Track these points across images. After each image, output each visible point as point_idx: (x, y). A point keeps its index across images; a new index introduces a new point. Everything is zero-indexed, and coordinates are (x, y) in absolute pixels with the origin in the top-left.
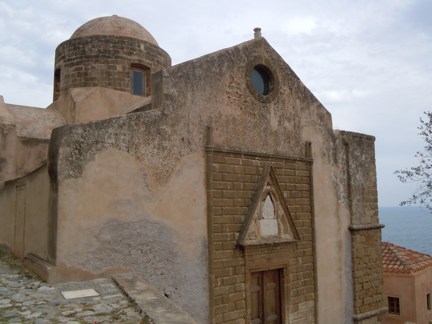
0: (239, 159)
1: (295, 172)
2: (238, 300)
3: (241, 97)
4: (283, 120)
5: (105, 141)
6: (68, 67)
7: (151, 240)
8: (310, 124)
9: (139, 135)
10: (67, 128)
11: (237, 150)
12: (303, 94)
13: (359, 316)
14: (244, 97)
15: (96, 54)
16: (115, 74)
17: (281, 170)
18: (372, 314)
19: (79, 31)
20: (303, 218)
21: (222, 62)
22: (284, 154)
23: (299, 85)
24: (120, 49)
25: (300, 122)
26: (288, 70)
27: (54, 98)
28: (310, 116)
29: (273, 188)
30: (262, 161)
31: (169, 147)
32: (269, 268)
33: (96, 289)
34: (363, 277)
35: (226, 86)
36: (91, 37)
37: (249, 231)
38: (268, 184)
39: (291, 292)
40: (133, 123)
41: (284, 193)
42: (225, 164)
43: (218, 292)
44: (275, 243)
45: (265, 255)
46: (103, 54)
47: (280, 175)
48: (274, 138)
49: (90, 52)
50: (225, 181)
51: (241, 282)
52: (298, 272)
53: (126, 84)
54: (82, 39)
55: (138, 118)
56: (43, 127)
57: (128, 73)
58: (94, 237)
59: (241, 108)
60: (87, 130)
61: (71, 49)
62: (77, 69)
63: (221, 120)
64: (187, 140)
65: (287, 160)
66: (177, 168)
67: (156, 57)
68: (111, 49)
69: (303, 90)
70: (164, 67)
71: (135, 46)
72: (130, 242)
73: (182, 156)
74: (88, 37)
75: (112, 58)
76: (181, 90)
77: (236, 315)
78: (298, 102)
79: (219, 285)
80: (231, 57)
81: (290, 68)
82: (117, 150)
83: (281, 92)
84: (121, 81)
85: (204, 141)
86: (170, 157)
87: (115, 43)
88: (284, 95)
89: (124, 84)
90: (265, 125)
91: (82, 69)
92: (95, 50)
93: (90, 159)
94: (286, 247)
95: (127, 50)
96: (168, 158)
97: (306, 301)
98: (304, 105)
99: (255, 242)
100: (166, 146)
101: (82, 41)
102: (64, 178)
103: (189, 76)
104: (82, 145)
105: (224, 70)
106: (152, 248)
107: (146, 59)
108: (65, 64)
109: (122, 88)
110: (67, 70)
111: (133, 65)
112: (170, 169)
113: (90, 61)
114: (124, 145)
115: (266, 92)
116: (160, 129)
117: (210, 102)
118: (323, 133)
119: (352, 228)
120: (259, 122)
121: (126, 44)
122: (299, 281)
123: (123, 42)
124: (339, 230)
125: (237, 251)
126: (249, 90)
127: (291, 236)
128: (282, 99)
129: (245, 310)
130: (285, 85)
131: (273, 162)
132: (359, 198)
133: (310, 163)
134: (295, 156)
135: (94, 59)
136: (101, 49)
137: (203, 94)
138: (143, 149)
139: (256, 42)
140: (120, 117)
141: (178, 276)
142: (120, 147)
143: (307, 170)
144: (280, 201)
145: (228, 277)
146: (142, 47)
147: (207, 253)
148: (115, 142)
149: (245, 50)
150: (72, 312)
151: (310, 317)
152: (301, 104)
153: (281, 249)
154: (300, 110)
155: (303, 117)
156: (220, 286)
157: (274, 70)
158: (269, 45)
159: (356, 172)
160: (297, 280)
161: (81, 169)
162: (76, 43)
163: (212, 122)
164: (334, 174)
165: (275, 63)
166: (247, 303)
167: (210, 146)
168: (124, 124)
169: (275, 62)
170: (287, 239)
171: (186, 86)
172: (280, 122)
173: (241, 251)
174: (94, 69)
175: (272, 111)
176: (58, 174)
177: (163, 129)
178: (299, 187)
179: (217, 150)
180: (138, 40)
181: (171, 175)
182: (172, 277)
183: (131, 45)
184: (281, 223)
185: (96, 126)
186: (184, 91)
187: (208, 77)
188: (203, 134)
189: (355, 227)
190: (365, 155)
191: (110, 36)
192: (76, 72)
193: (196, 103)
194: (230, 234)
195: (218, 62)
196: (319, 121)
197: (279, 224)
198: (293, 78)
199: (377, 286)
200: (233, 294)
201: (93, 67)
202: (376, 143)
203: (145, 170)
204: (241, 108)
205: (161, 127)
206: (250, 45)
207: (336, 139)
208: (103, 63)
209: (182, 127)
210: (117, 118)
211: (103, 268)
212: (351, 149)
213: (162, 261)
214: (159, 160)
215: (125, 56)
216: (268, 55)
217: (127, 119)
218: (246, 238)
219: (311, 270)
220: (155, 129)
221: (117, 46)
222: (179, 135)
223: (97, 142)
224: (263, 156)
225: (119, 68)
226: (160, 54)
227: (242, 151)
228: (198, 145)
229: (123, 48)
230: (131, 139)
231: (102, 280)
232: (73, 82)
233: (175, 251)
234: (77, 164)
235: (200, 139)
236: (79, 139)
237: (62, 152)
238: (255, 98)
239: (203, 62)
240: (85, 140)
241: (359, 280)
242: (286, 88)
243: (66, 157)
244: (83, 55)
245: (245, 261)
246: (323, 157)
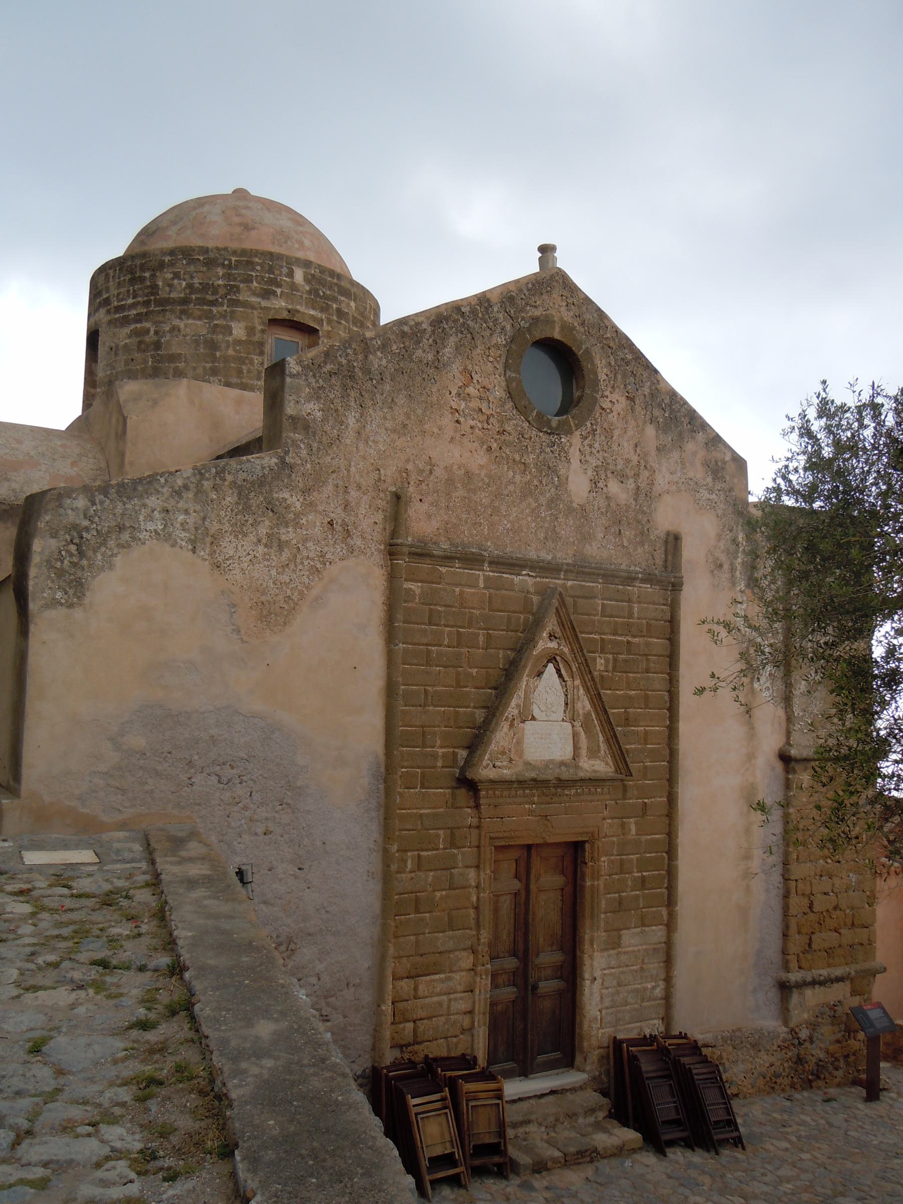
0: (477, 572)
1: (631, 609)
2: (459, 909)
3: (491, 420)
4: (603, 477)
5: (140, 524)
6: (116, 327)
7: (242, 755)
8: (683, 488)
9: (222, 513)
10: (52, 495)
12: (665, 412)
13: (795, 976)
14: (498, 421)
15: (182, 295)
16: (228, 347)
17: (592, 601)
18: (833, 976)
19: (147, 234)
20: (645, 724)
21: (443, 335)
22: (602, 564)
23: (657, 389)
24: (241, 281)
26: (626, 351)
27: (83, 402)
28: (683, 468)
29: (564, 646)
30: (538, 579)
31: (294, 542)
32: (543, 838)
33: (98, 851)
34: (814, 881)
35: (450, 393)
36: (172, 253)
37: (493, 747)
38: (551, 636)
39: (603, 902)
40: (207, 484)
41: (595, 659)
42: (439, 584)
43: (407, 884)
44: (559, 779)
45: (534, 806)
46: (198, 296)
47: (589, 615)
48: (578, 522)
49: (167, 289)
50: (437, 625)
51: (467, 867)
52: (624, 855)
53: (255, 372)
54: (149, 257)
55: (220, 473)
56: (48, 478)
58: (109, 739)
59: (489, 449)
60: (97, 501)
61: (125, 280)
62: (136, 333)
63: (432, 477)
64: (341, 525)
65: (609, 576)
67: (335, 300)
68: (220, 282)
70: (356, 326)
71: (280, 275)
73: (328, 564)
74: (164, 253)
75: (222, 305)
76: (332, 406)
77: (451, 942)
78: (650, 431)
79: (408, 870)
82: (167, 547)
84: (243, 363)
85: (385, 529)
86: (296, 566)
87: (230, 266)
89: (249, 371)
90: (553, 490)
91: (147, 331)
92: (180, 284)
93: (104, 566)
94: (593, 790)
96: (292, 566)
97: (644, 925)
100: (288, 539)
102: (42, 607)
104: (85, 535)
105: (448, 355)
106: (243, 774)
107: (307, 307)
108: (109, 318)
109: (244, 381)
110: (114, 334)
112: (296, 594)
113: (168, 313)
114: (183, 534)
116: (273, 498)
117: (405, 434)
118: (720, 512)
119: (788, 754)
120: (536, 483)
121: (258, 268)
122: (627, 876)
123: (250, 264)
124: (751, 757)
125: (462, 792)
126: (512, 404)
127: (607, 764)
128: (605, 425)
129: (474, 933)
130: (614, 390)
131: (570, 583)
133: (676, 587)
136: (194, 283)
137: (388, 416)
138: (229, 547)
139: (538, 282)
140: (177, 471)
141: (306, 840)
142: (175, 541)
143: (664, 605)
145: (434, 852)
146: (299, 275)
147: (382, 792)
148: (163, 530)
150: (25, 886)
151: (652, 966)
152: (657, 437)
153: (577, 794)
154: (653, 452)
155: (664, 469)
156: (411, 872)
158: (576, 286)
160: (621, 873)
161: (82, 587)
162: (136, 267)
166: (481, 917)
167: (400, 541)
168: (186, 487)
169: (591, 331)
170: (595, 771)
171: (345, 396)
172: (595, 483)
173: (471, 793)
174: (176, 333)
175: (574, 455)
176: (30, 598)
178: (639, 645)
179: (419, 551)
180: (287, 257)
181: (297, 607)
182: (292, 841)
183: (271, 270)
184: (583, 733)
185: (118, 492)
186: (340, 408)
188: (383, 511)
189: (793, 752)
191: (217, 248)
192: (135, 340)
193: (369, 438)
194: (443, 753)
195: (430, 337)
196: (709, 479)
197: (575, 736)
200: (444, 893)
201: (175, 329)
203: (232, 593)
204: (489, 449)
205: (277, 496)
206: (520, 290)
208: (200, 318)
210: (171, 473)
211: (127, 810)
213: (267, 804)
214: (269, 571)
215: (254, 299)
216: (572, 314)
217: (194, 475)
218: (484, 763)
219: (663, 852)
221: (234, 274)
222: (320, 513)
223: (121, 528)
224: (541, 568)
225: (239, 331)
226: (346, 293)
227: (485, 554)
229: (248, 280)
231: (121, 834)
232: (127, 363)
233: (299, 783)
234: (72, 577)
235: (376, 523)
236: (78, 522)
237: (39, 550)
238: (529, 422)
239: (393, 337)
240: (92, 523)
241: (800, 885)
243: (47, 561)
244: (152, 298)
245: (480, 818)
246: (716, 572)
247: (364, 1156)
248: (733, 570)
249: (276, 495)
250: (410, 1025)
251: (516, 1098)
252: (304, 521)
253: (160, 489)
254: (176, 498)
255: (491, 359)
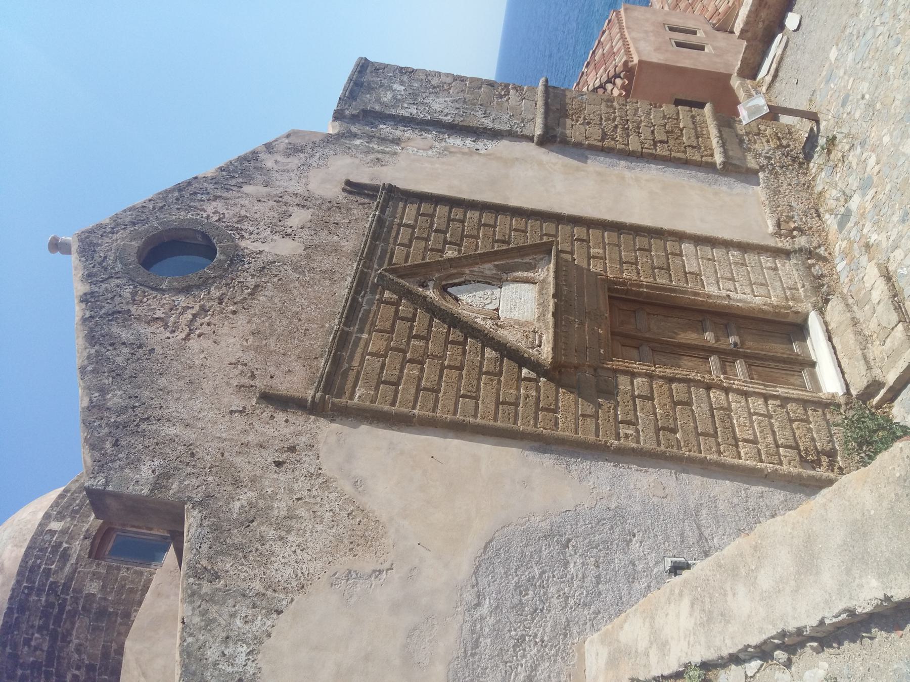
1: (406, 225)
4: (282, 228)
5: (237, 672)
11: (331, 338)
15: (48, 638)
16: (105, 599)
24: (47, 579)
25: (297, 194)
26: (170, 195)
29: (433, 276)
35: (169, 338)
37: (522, 345)
40: (206, 588)
46: (52, 622)
48: (320, 253)
49: (38, 653)
57: (110, 568)
59: (234, 313)
66: (348, 488)
68: (43, 599)
69: (224, 174)
72: (511, 637)
73: (320, 471)
75: (65, 600)
78: (247, 189)
80: (101, 313)
81: (166, 191)
82: (268, 642)
83: (217, 218)
84: (124, 586)
86: (317, 503)
88: (227, 215)
89: (132, 582)
90: (286, 267)
92: (36, 639)
95: (54, 562)
96: (316, 508)
98: (259, 178)
99: (548, 338)
100: (285, 509)
101: (7, 667)
103: (120, 423)
111: (94, 554)
114: (258, 622)
115: (209, 251)
116: (237, 519)
118: (332, 153)
120: (276, 279)
123: (33, 570)
127: (542, 259)
131: (376, 266)
132: (480, 112)
133: (391, 190)
134: (370, 219)
135: (59, 643)
137: (176, 396)
138: (281, 572)
139: (82, 252)
144: (465, 266)
146: (55, 526)
148: (249, 645)
149: (95, 279)
154: (266, 189)
157: (160, 224)
159: (427, 108)
163: (252, 386)
164: (424, 150)
165: (144, 222)
167: (310, 399)
168: (204, 613)
171: (143, 434)
175: (259, 246)
177: (241, 511)
178: (439, 224)
180: (35, 534)
186: (155, 441)
187: (135, 377)
189: (538, 132)
190: (394, 83)
196: (302, 155)
198: (192, 189)
199: (662, 115)
201: (78, 650)
202: (375, 57)
207: (350, 132)
208: (73, 623)
209: (247, 460)
212: (377, 107)
215: (67, 569)
217: (191, 602)
218: (536, 353)
220: (236, 531)
221: (39, 585)
228: (300, 428)
229: (48, 572)
230: (248, 601)
235: (287, 421)
241: (646, 146)
242: (210, 208)
244: (44, 668)
246: (383, 163)
247: (705, 619)
248: (383, 152)
249: (235, 515)
250: (781, 450)
251: (839, 369)
252: (269, 491)
253: (200, 643)
254: (213, 625)
255: (145, 299)
